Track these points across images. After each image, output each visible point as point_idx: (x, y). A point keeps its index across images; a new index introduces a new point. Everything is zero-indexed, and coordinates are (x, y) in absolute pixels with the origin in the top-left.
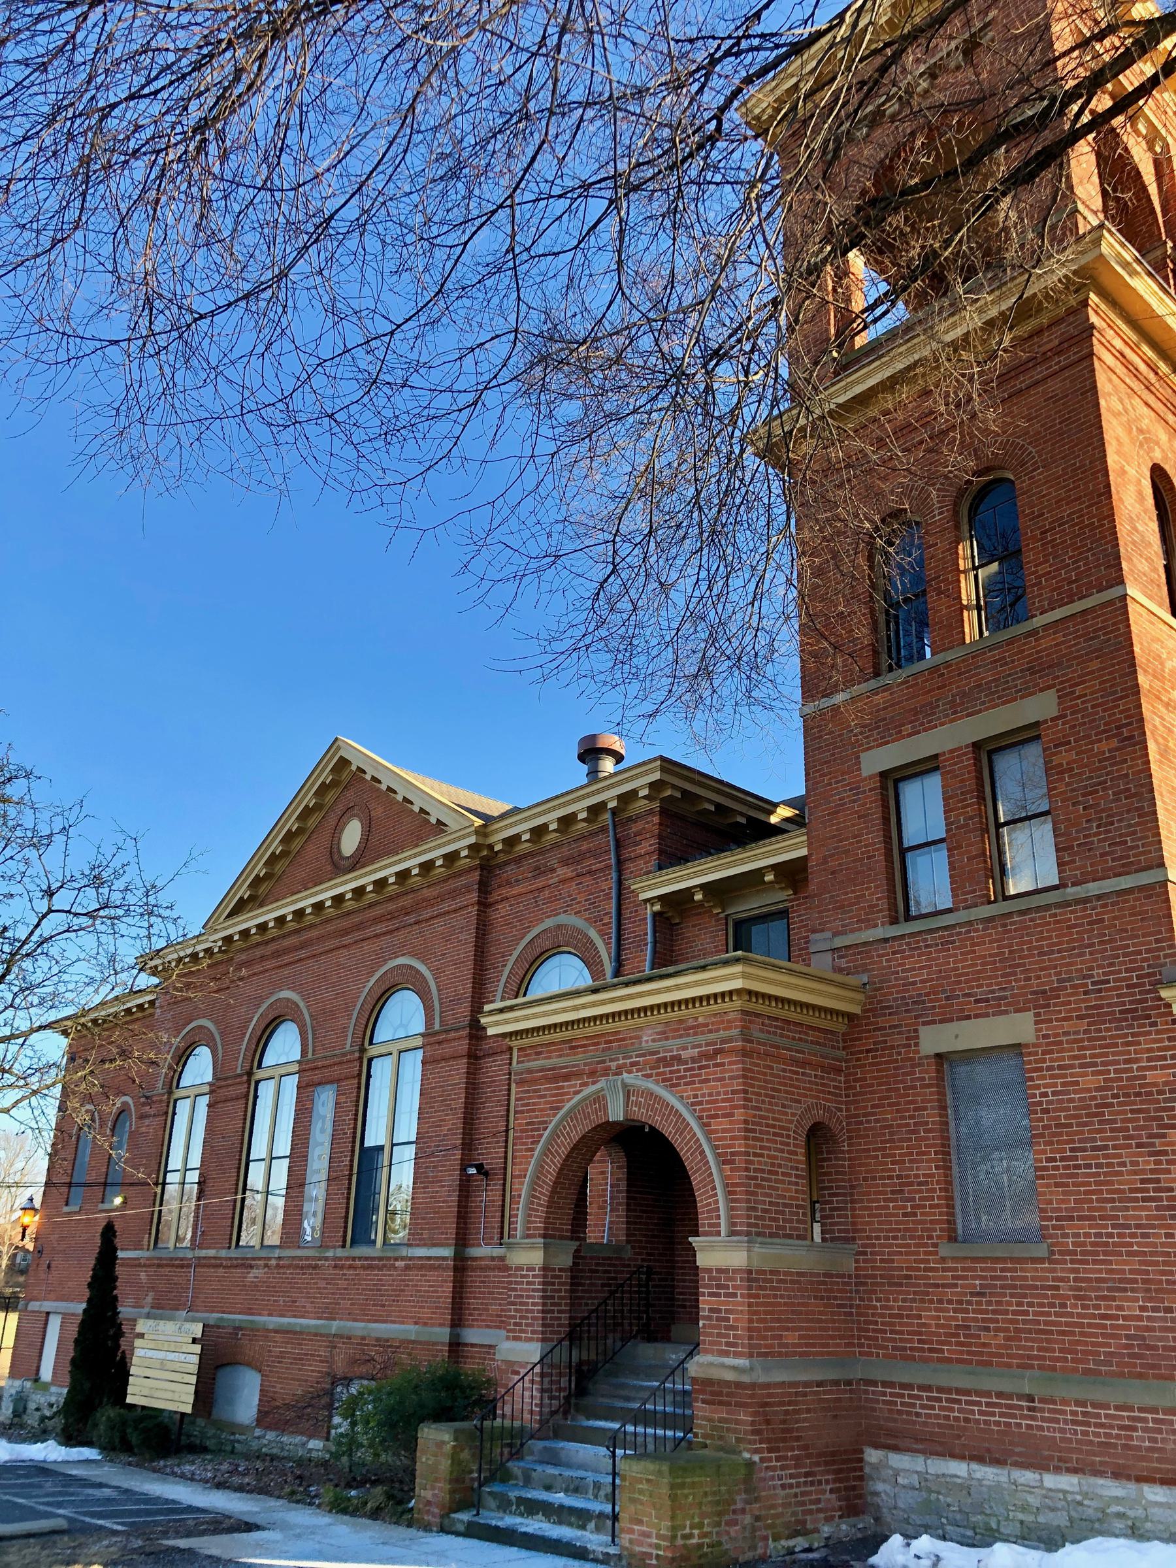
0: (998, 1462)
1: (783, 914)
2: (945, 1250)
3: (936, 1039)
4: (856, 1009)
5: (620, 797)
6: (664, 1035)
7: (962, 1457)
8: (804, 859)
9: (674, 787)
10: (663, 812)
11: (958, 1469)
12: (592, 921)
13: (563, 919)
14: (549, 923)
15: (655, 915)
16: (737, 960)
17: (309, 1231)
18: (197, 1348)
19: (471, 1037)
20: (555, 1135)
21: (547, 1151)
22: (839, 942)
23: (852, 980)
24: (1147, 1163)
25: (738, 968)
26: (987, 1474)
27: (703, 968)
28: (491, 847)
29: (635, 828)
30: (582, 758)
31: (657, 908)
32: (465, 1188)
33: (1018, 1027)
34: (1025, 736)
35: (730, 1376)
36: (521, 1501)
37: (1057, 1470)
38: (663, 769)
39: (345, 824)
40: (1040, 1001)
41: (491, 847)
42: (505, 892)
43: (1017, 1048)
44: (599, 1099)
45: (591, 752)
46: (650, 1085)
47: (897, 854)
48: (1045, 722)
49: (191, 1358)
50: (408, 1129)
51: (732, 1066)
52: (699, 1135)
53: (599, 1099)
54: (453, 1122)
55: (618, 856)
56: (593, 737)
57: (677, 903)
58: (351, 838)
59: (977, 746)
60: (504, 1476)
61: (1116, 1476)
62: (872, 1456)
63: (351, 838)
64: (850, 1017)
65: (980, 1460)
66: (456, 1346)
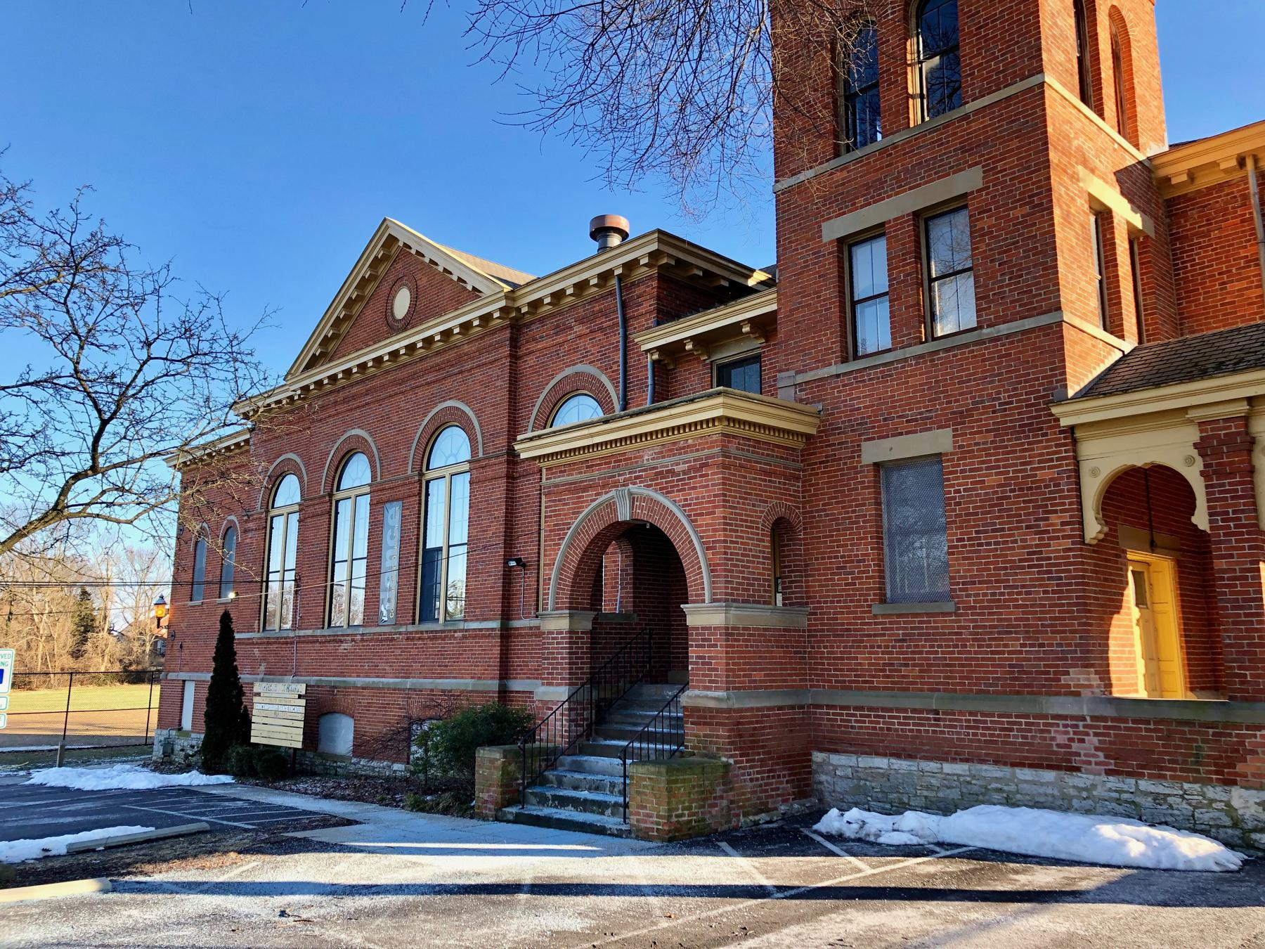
0: (910, 757)
1: (756, 359)
2: (876, 609)
3: (873, 452)
4: (813, 431)
5: (625, 265)
6: (661, 455)
7: (885, 755)
8: (774, 313)
9: (670, 256)
10: (661, 277)
11: (881, 763)
12: (604, 369)
13: (580, 368)
14: (569, 371)
15: (654, 362)
16: (719, 394)
17: (385, 613)
18: (303, 702)
19: (508, 462)
20: (577, 533)
21: (569, 547)
22: (800, 379)
23: (809, 408)
24: (1033, 540)
25: (720, 400)
26: (902, 765)
27: (692, 401)
28: (519, 309)
29: (638, 291)
30: (594, 235)
31: (656, 357)
32: (508, 578)
33: (940, 440)
34: (957, 204)
35: (712, 704)
36: (555, 797)
37: (954, 760)
38: (660, 240)
39: (397, 292)
40: (957, 420)
41: (519, 309)
42: (532, 346)
43: (938, 457)
44: (611, 505)
45: (601, 231)
46: (651, 493)
47: (848, 307)
48: (972, 193)
49: (298, 710)
50: (461, 533)
51: (714, 477)
52: (689, 528)
53: (611, 505)
54: (497, 528)
55: (624, 315)
56: (602, 218)
57: (672, 352)
58: (402, 303)
59: (916, 214)
60: (544, 782)
61: (996, 762)
62: (818, 757)
63: (402, 303)
64: (808, 437)
65: (898, 756)
66: (504, 693)
